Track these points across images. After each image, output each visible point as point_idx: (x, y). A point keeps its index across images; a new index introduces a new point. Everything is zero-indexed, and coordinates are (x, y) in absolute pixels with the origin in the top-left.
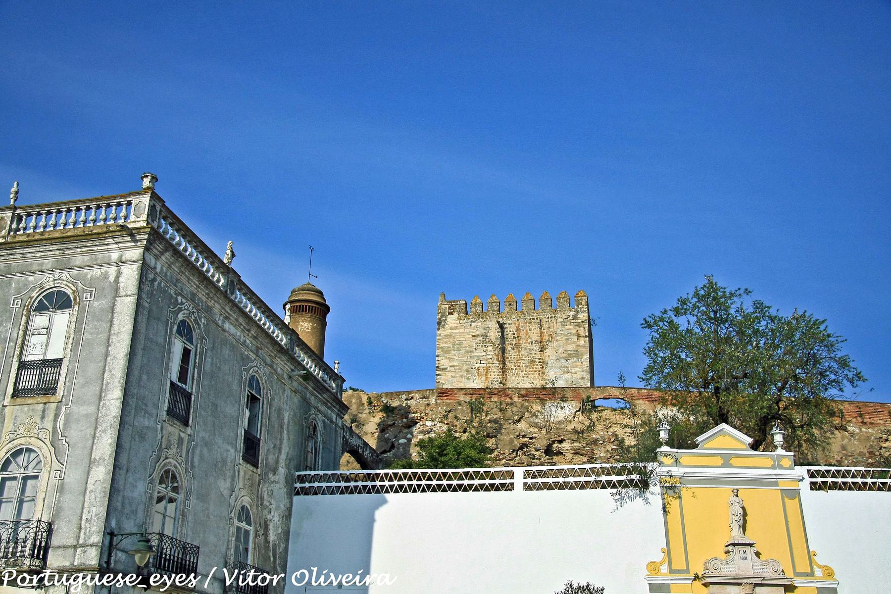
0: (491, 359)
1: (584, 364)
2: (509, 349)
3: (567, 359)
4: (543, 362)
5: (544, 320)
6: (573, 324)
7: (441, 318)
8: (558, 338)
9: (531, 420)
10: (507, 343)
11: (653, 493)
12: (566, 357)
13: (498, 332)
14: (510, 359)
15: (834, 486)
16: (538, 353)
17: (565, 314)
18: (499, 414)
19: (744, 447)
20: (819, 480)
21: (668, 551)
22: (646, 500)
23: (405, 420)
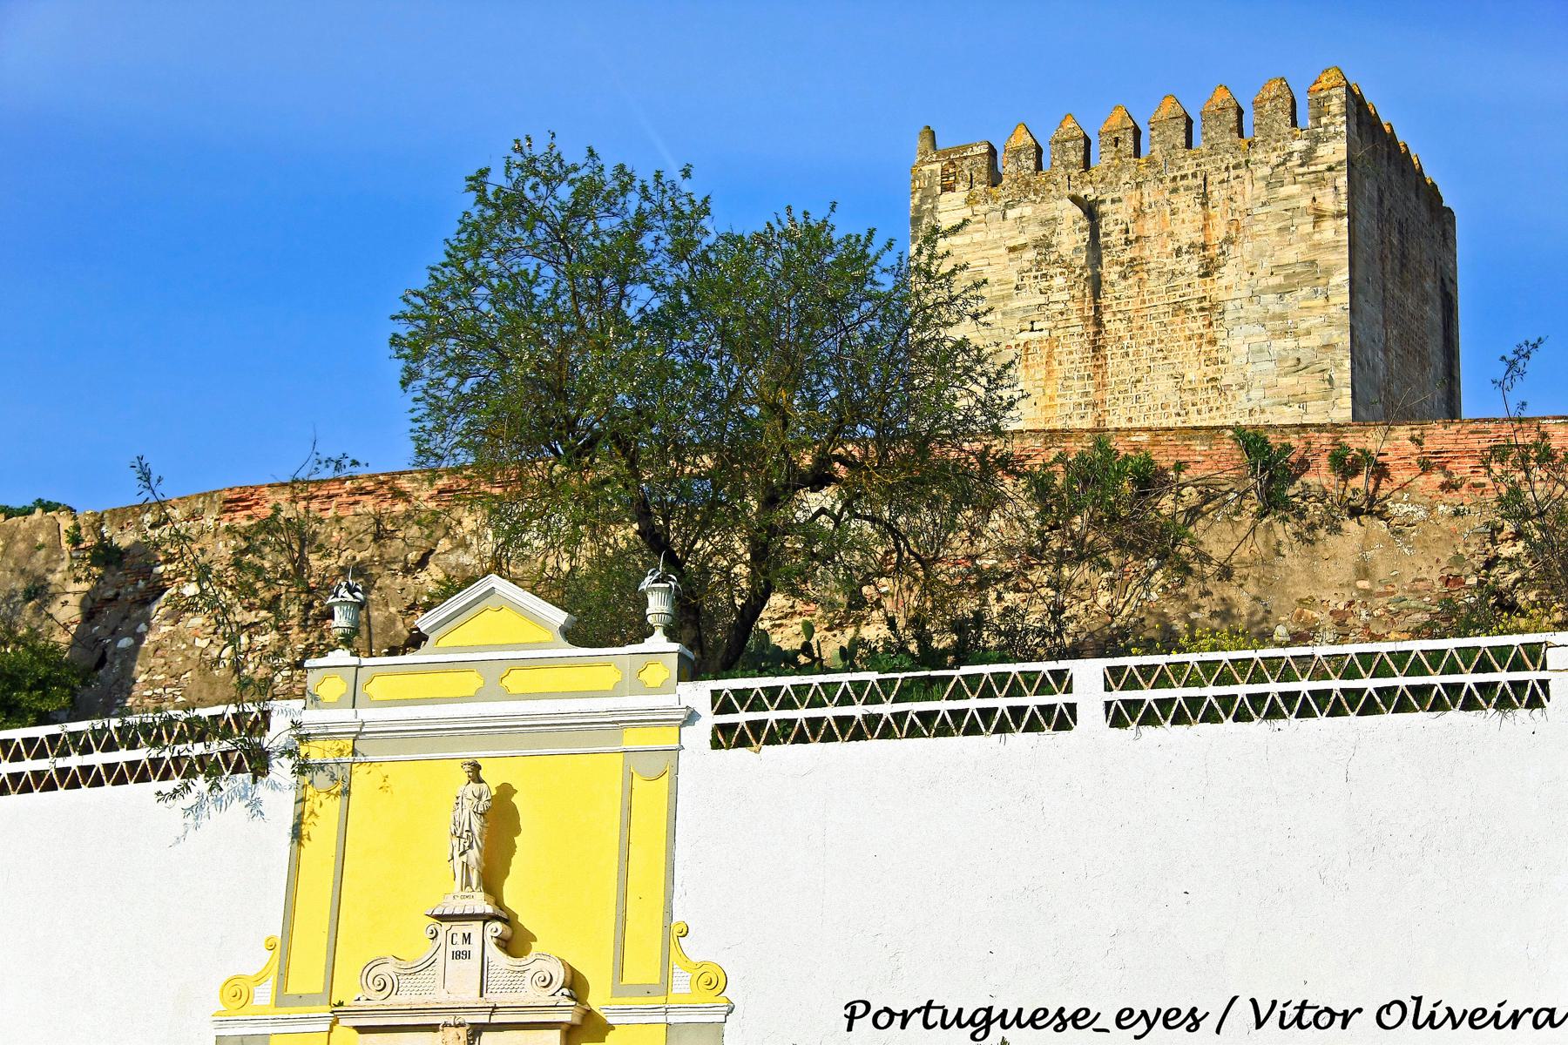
0: (1062, 314)
1: (1333, 300)
2: (1114, 277)
3: (1282, 292)
4: (1213, 307)
5: (1214, 178)
6: (1300, 179)
7: (920, 206)
8: (1255, 229)
9: (452, 559)
10: (1105, 260)
11: (274, 786)
12: (1280, 286)
13: (1081, 230)
14: (1115, 309)
15: (784, 733)
16: (1197, 280)
17: (1279, 152)
18: (370, 550)
19: (546, 636)
20: (742, 717)
21: (284, 947)
22: (255, 805)
23: (141, 584)
